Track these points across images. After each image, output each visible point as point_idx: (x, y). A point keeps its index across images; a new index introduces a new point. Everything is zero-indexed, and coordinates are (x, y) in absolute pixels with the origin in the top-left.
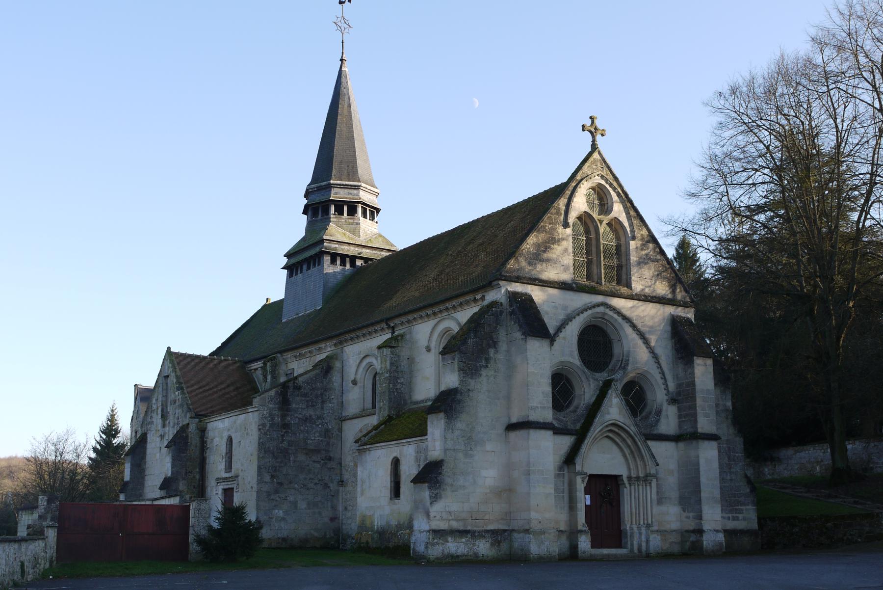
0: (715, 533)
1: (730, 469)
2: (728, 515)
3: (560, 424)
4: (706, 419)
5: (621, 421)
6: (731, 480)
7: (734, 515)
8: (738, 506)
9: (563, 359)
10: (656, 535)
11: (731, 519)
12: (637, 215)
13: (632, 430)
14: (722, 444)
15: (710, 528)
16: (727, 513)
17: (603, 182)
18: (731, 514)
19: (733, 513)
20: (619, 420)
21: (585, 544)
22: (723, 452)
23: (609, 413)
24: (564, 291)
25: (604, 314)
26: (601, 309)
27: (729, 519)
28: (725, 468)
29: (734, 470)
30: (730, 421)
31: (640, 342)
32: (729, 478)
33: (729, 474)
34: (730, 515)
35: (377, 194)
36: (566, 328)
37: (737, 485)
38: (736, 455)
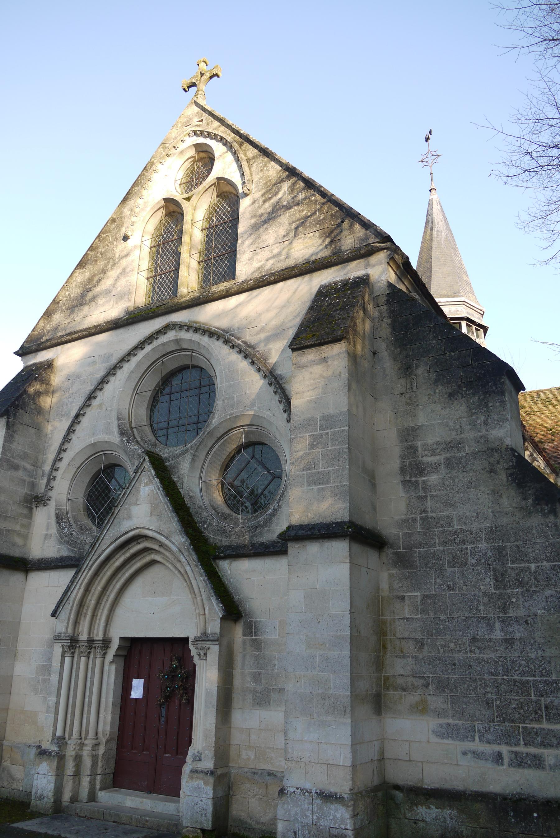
0: (319, 801)
1: (504, 609)
2: (496, 748)
3: (73, 550)
4: (316, 488)
5: (152, 528)
6: (509, 642)
7: (522, 749)
8: (538, 720)
9: (92, 440)
10: (201, 783)
11: (506, 760)
12: (260, 151)
13: (173, 543)
14: (472, 542)
15: (308, 786)
16: (489, 742)
17: (201, 140)
18: (507, 744)
19: (517, 744)
20: (148, 527)
21: (45, 781)
22: (478, 564)
23: (129, 517)
24: (128, 328)
25: (177, 341)
26: (171, 335)
27: (498, 758)
28: (482, 607)
29: (522, 612)
30: (503, 477)
31: (244, 364)
32: (498, 634)
33: (498, 625)
34: (505, 749)
35: (482, 313)
36: (104, 390)
37: (533, 656)
38: (529, 568)
